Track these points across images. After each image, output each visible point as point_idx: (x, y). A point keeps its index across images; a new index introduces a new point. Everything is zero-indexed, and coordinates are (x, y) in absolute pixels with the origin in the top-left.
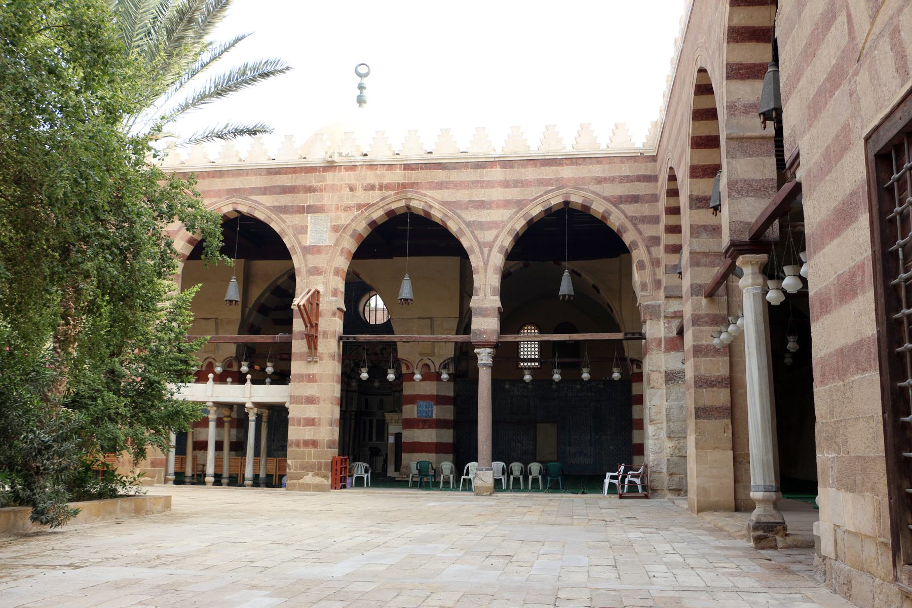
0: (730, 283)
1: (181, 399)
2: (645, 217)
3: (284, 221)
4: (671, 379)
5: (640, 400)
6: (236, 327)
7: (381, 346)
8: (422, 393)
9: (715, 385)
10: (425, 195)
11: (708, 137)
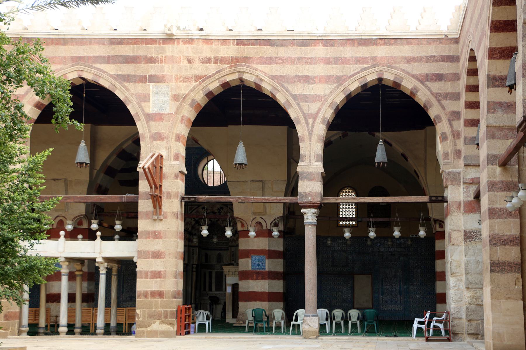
0: (521, 154)
1: (34, 255)
2: (448, 93)
3: (128, 90)
4: (469, 238)
5: (442, 255)
6: (85, 188)
7: (218, 206)
8: (255, 248)
9: (507, 244)
10: (256, 69)
11: (506, 21)
